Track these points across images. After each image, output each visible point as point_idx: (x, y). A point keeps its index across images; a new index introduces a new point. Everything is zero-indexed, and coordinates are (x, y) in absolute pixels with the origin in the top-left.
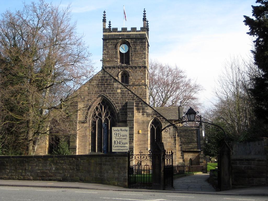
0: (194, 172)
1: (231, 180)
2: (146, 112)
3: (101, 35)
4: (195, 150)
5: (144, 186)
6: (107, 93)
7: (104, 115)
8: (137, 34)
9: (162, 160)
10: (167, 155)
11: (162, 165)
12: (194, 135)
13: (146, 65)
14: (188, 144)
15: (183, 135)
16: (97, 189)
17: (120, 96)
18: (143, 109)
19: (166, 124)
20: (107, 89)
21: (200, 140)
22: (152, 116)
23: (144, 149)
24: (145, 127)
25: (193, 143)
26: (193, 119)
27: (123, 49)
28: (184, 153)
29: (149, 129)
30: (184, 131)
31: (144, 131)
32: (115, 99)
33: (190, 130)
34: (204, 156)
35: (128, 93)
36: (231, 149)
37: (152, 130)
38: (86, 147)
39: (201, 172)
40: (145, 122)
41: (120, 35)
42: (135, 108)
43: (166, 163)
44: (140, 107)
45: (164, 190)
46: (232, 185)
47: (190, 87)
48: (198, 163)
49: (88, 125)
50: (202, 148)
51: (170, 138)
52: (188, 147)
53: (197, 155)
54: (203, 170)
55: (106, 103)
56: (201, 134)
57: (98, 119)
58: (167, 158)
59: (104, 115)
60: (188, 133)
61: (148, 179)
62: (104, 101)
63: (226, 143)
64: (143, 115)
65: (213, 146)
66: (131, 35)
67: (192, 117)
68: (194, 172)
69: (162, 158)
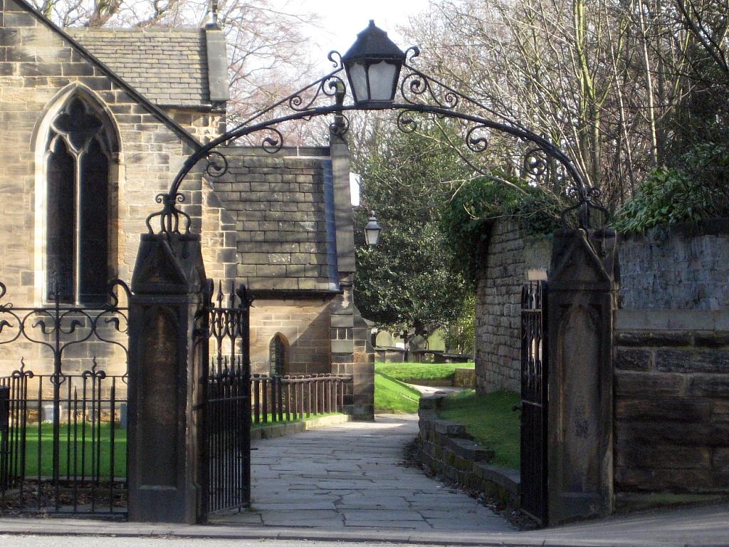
0: (305, 415)
1: (611, 459)
2: (23, 57)
4: (307, 285)
5: (74, 503)
9: (190, 342)
10: (221, 311)
11: (193, 372)
12: (300, 196)
14: (266, 247)
15: (235, 196)
16: (312, 527)
19: (141, 128)
21: (334, 228)
22: (61, 83)
23: (11, 276)
24: (18, 148)
25: (293, 242)
26: (385, 96)
29: (41, 160)
31: (9, 169)
33: (275, 167)
34: (357, 323)
36: (611, 278)
37: (60, 161)
39: (340, 411)
40: (14, 117)
43: (213, 354)
45: (201, 520)
46: (615, 491)
48: (324, 361)
50: (346, 274)
52: (267, 270)
53: (314, 311)
54: (349, 400)
56: (341, 189)
58: (217, 329)
60: (266, 187)
61: (48, 457)
63: (582, 240)
65: (386, 261)
67: (380, 77)
68: (305, 415)
69: (190, 332)
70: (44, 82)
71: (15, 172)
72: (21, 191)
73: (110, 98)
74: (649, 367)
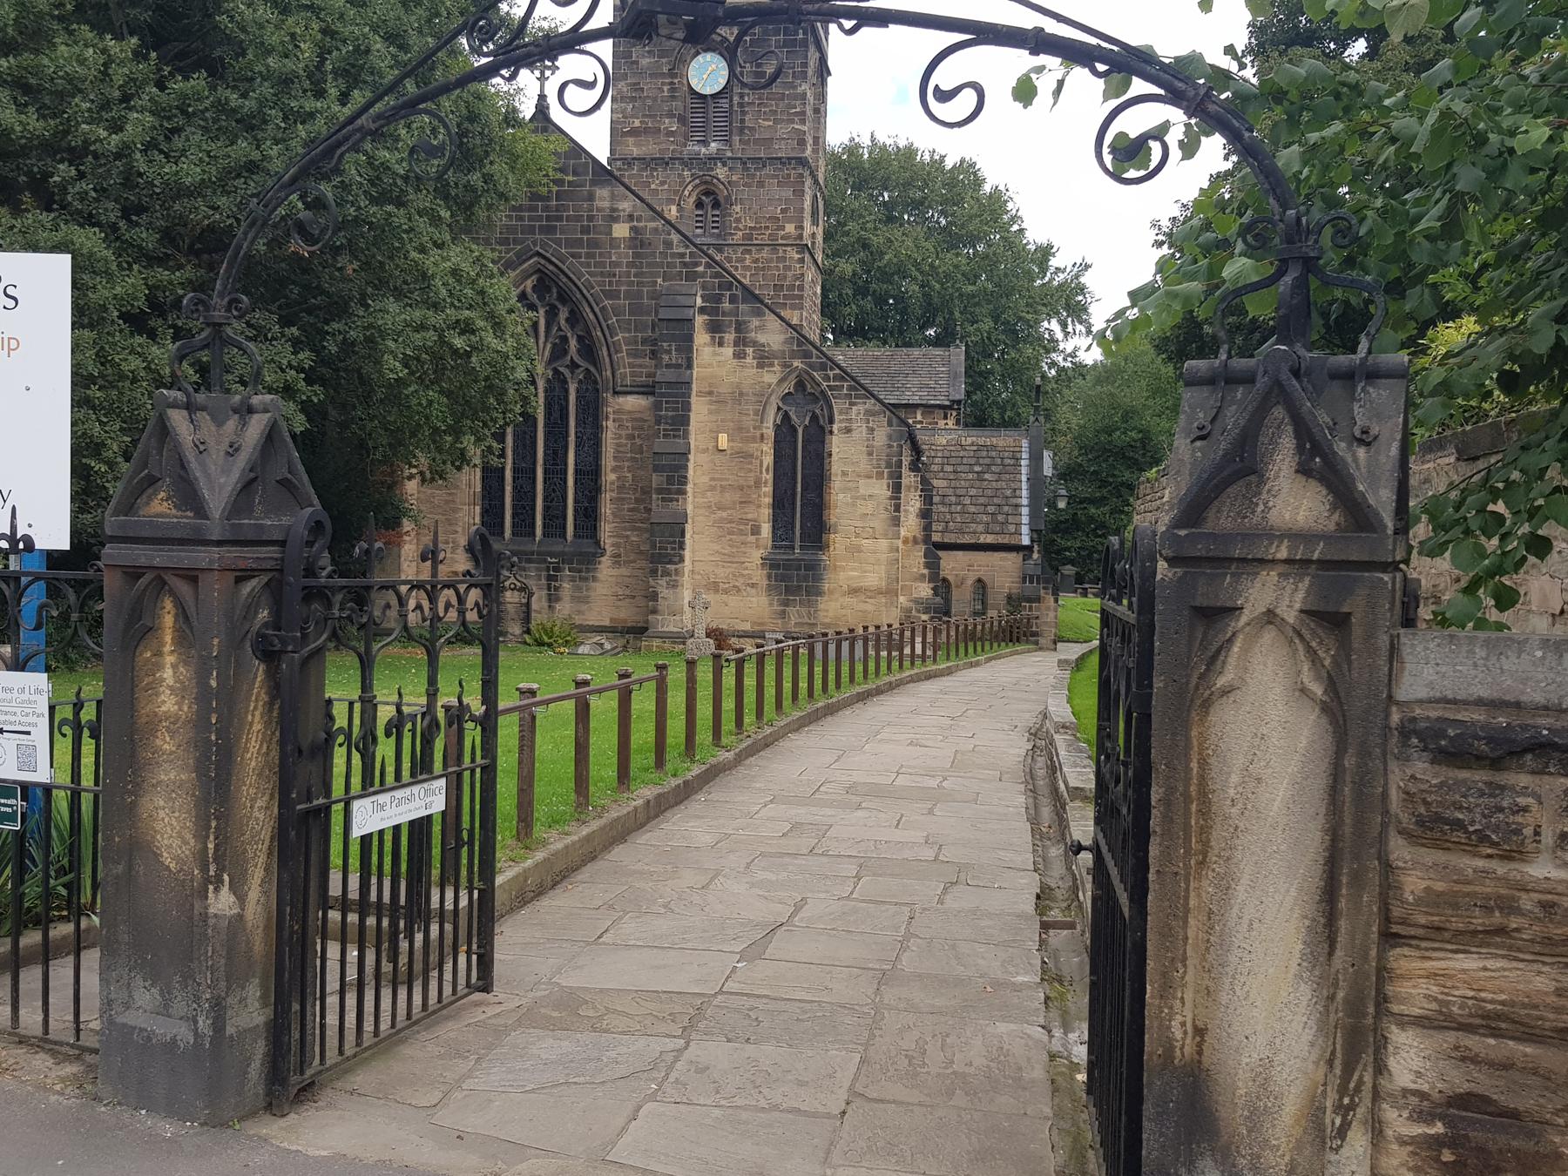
2: (755, 343)
13: (804, 151)
17: (624, 255)
19: (852, 404)
20: (560, 219)
22: (785, 366)
28: (940, 553)
35: (668, 244)
38: (455, 510)
42: (700, 320)
44: (724, 314)
59: (547, 353)
64: (739, 355)
70: (772, 365)
71: (746, 440)
72: (752, 456)
73: (827, 378)
74: (1531, 847)
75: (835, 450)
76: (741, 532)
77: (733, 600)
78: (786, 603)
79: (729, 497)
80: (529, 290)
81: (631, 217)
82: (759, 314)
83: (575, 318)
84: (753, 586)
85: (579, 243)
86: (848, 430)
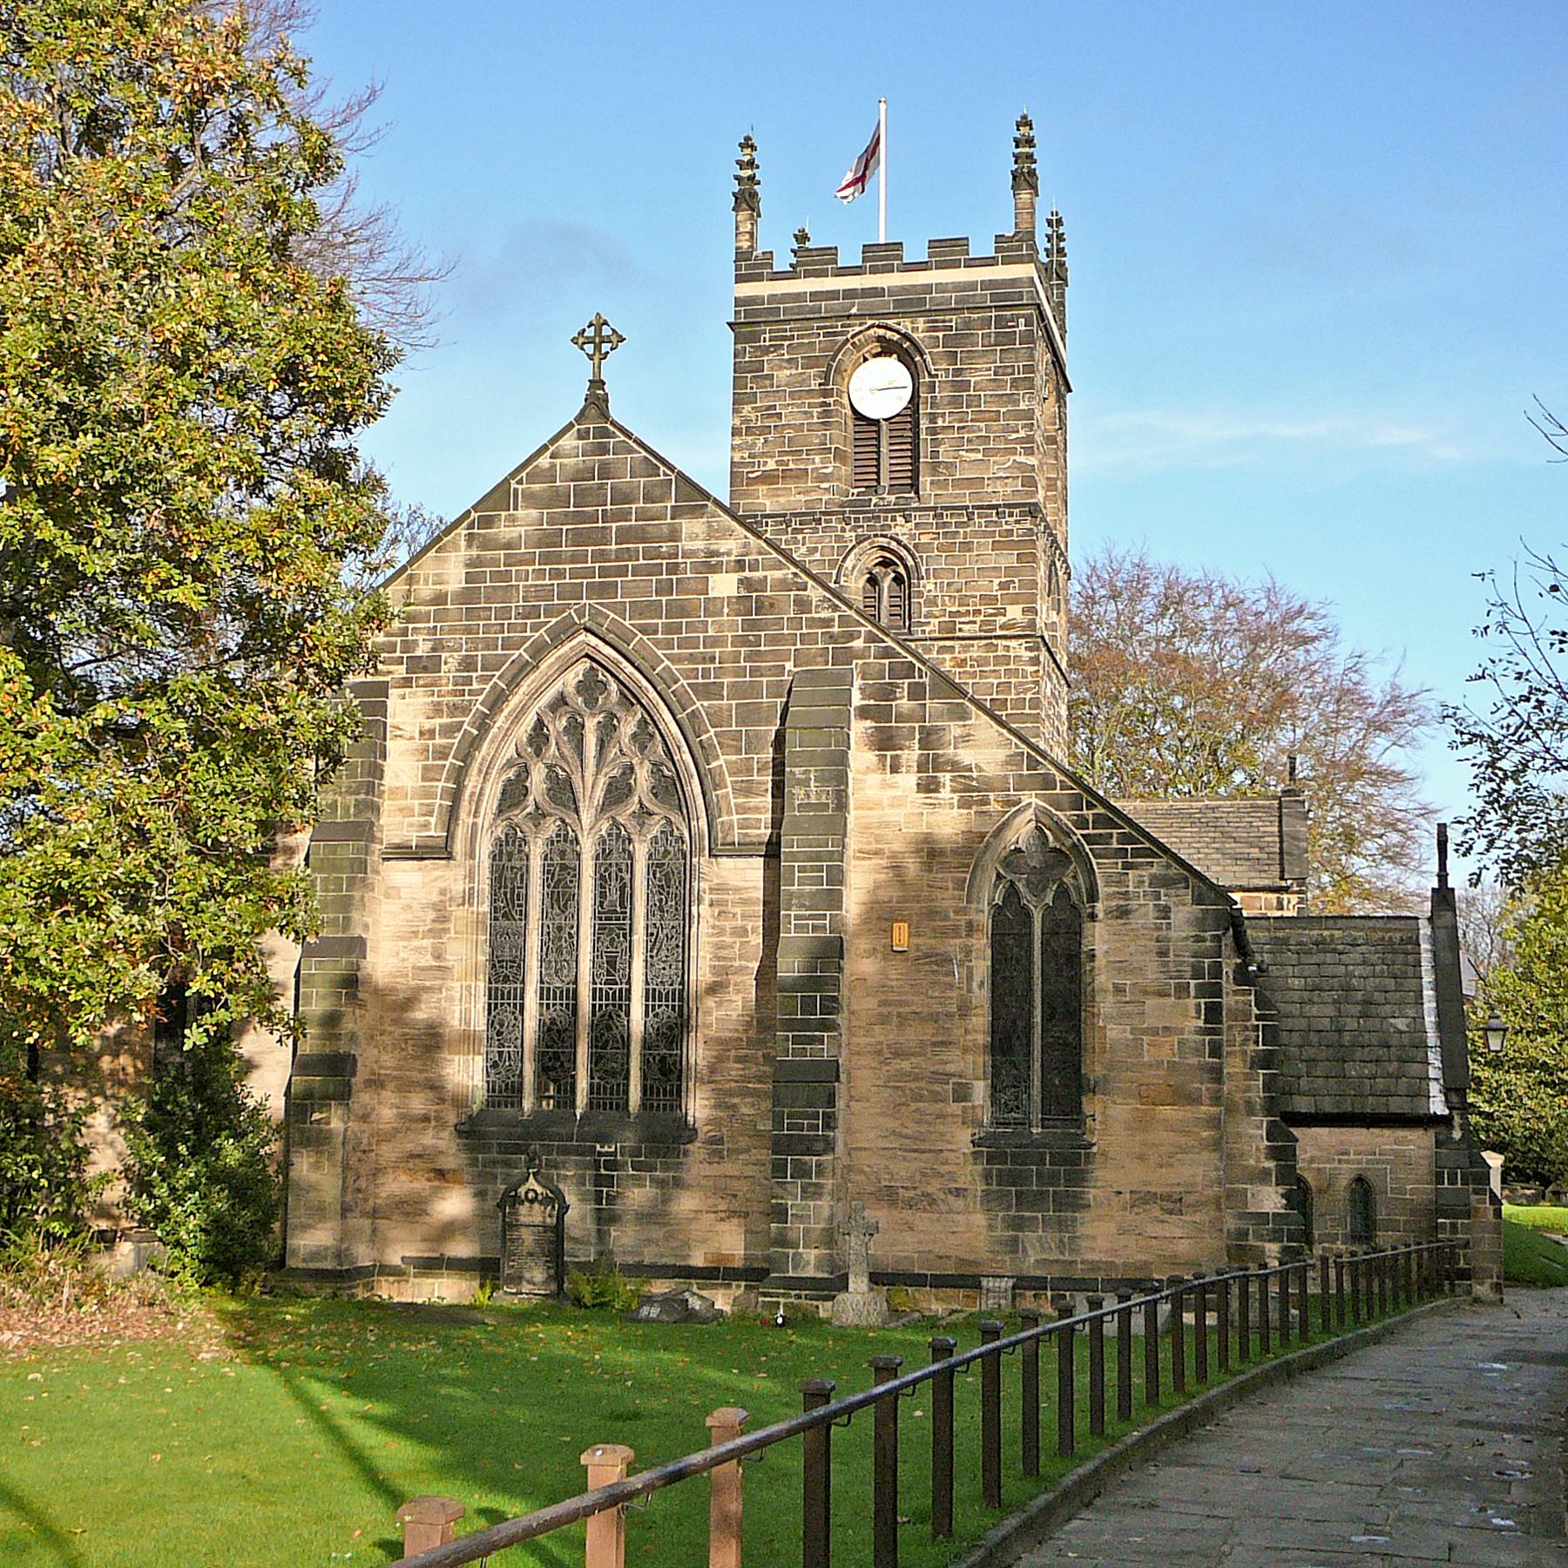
2: (955, 766)
3: (726, 293)
6: (619, 609)
7: (591, 787)
8: (972, 286)
17: (728, 625)
18: (928, 739)
19: (1127, 866)
20: (622, 572)
23: (937, 1087)
27: (879, 387)
28: (1295, 1131)
30: (1309, 952)
32: (692, 658)
35: (803, 605)
41: (850, 294)
42: (859, 729)
47: (1363, 702)
49: (466, 877)
51: (1163, 994)
55: (615, 697)
57: (551, 827)
62: (602, 675)
64: (928, 786)
66: (928, 288)
75: (1100, 948)
76: (937, 1098)
77: (922, 1220)
78: (1018, 1224)
79: (912, 1035)
80: (571, 689)
81: (740, 565)
82: (963, 716)
83: (646, 732)
84: (958, 1193)
85: (652, 609)
86: (1123, 913)
